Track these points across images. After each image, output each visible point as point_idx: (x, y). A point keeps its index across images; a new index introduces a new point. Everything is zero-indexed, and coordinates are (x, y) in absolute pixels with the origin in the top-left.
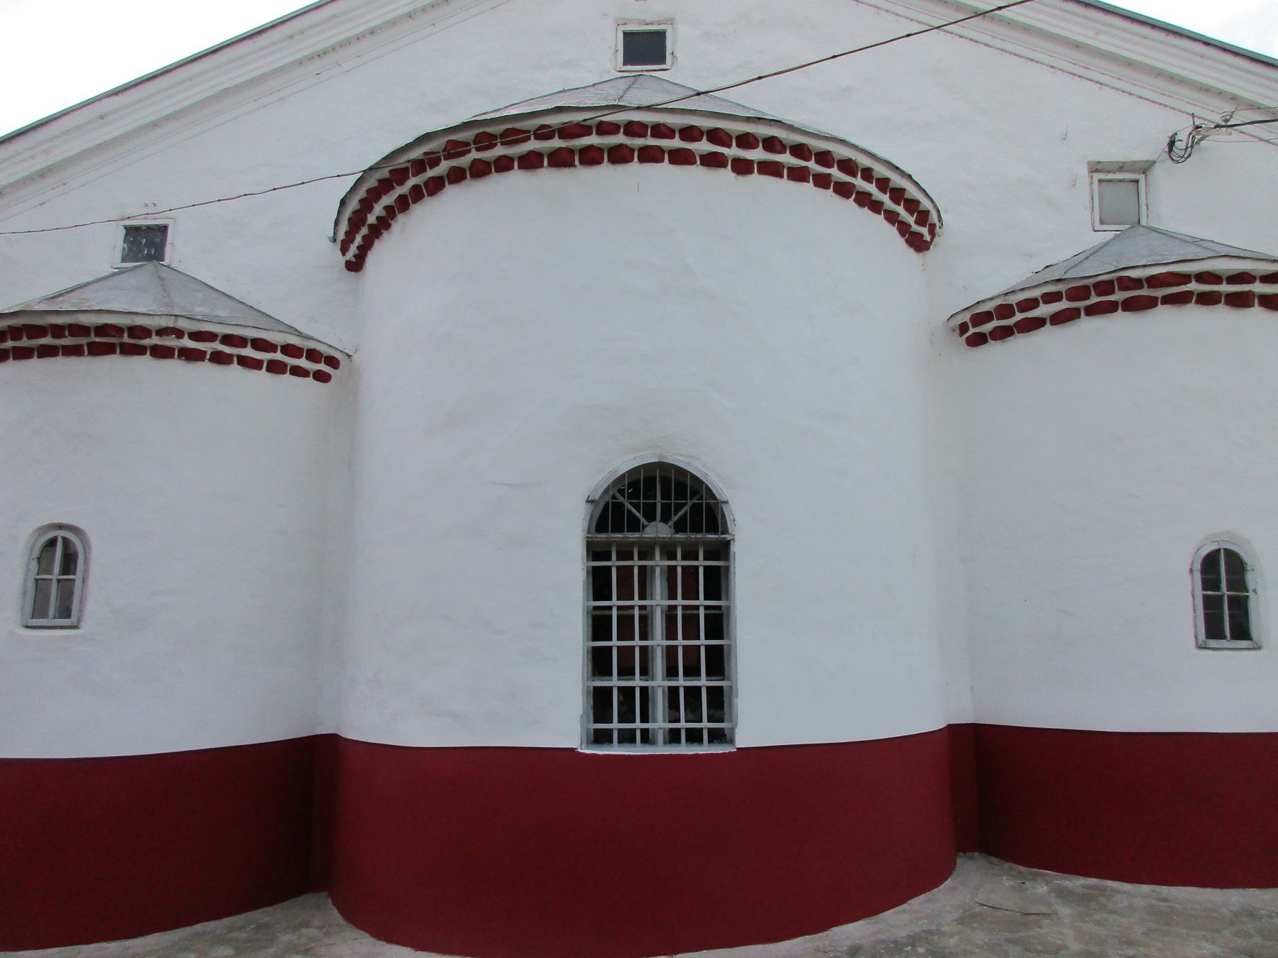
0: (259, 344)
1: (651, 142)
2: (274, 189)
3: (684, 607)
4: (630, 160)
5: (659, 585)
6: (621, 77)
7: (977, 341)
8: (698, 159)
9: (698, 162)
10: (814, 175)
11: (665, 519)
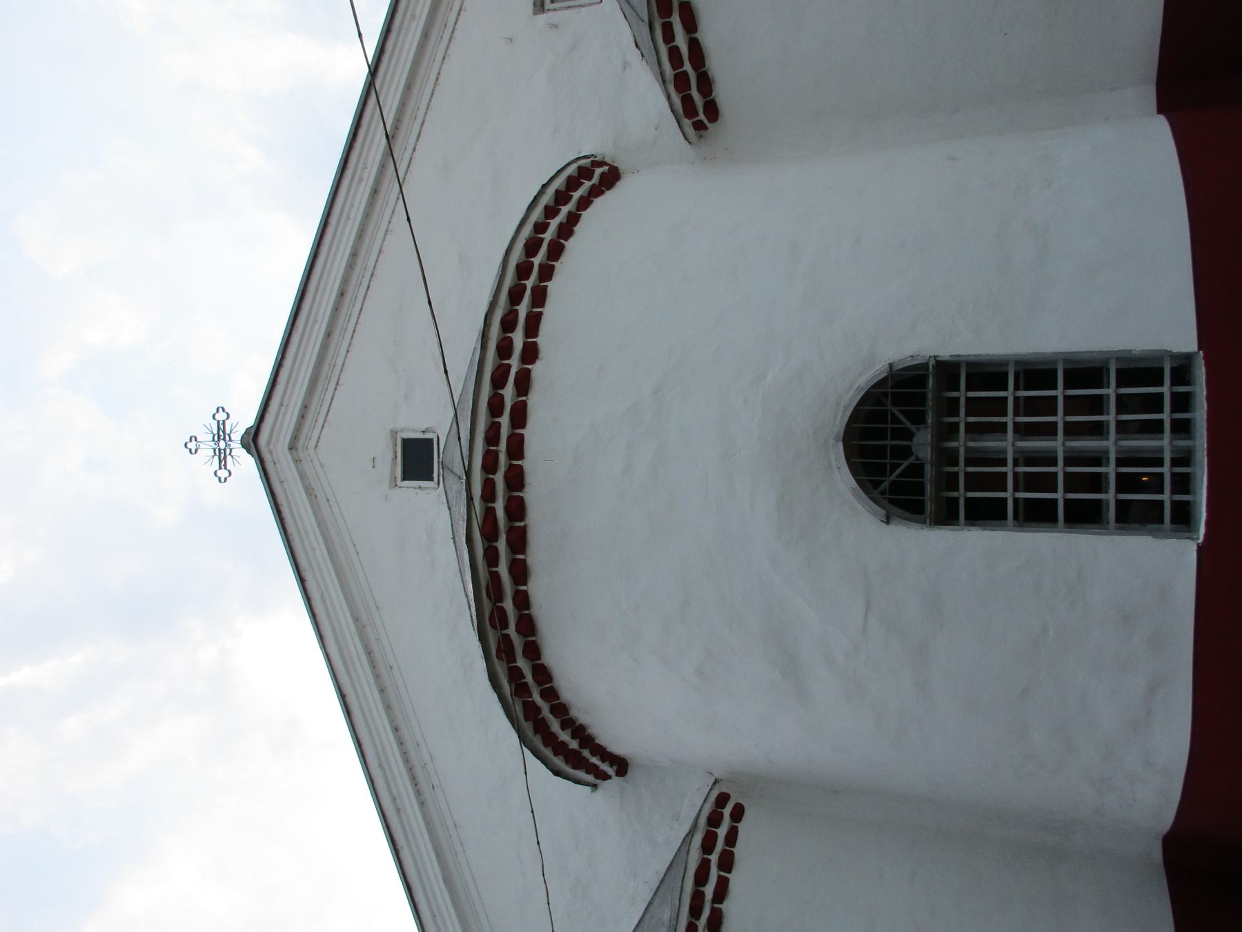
0: (701, 876)
1: (503, 446)
2: (538, 843)
3: (1016, 414)
4: (521, 468)
5: (990, 444)
6: (444, 482)
7: (713, 111)
8: (520, 399)
9: (524, 398)
10: (541, 282)
11: (909, 435)
